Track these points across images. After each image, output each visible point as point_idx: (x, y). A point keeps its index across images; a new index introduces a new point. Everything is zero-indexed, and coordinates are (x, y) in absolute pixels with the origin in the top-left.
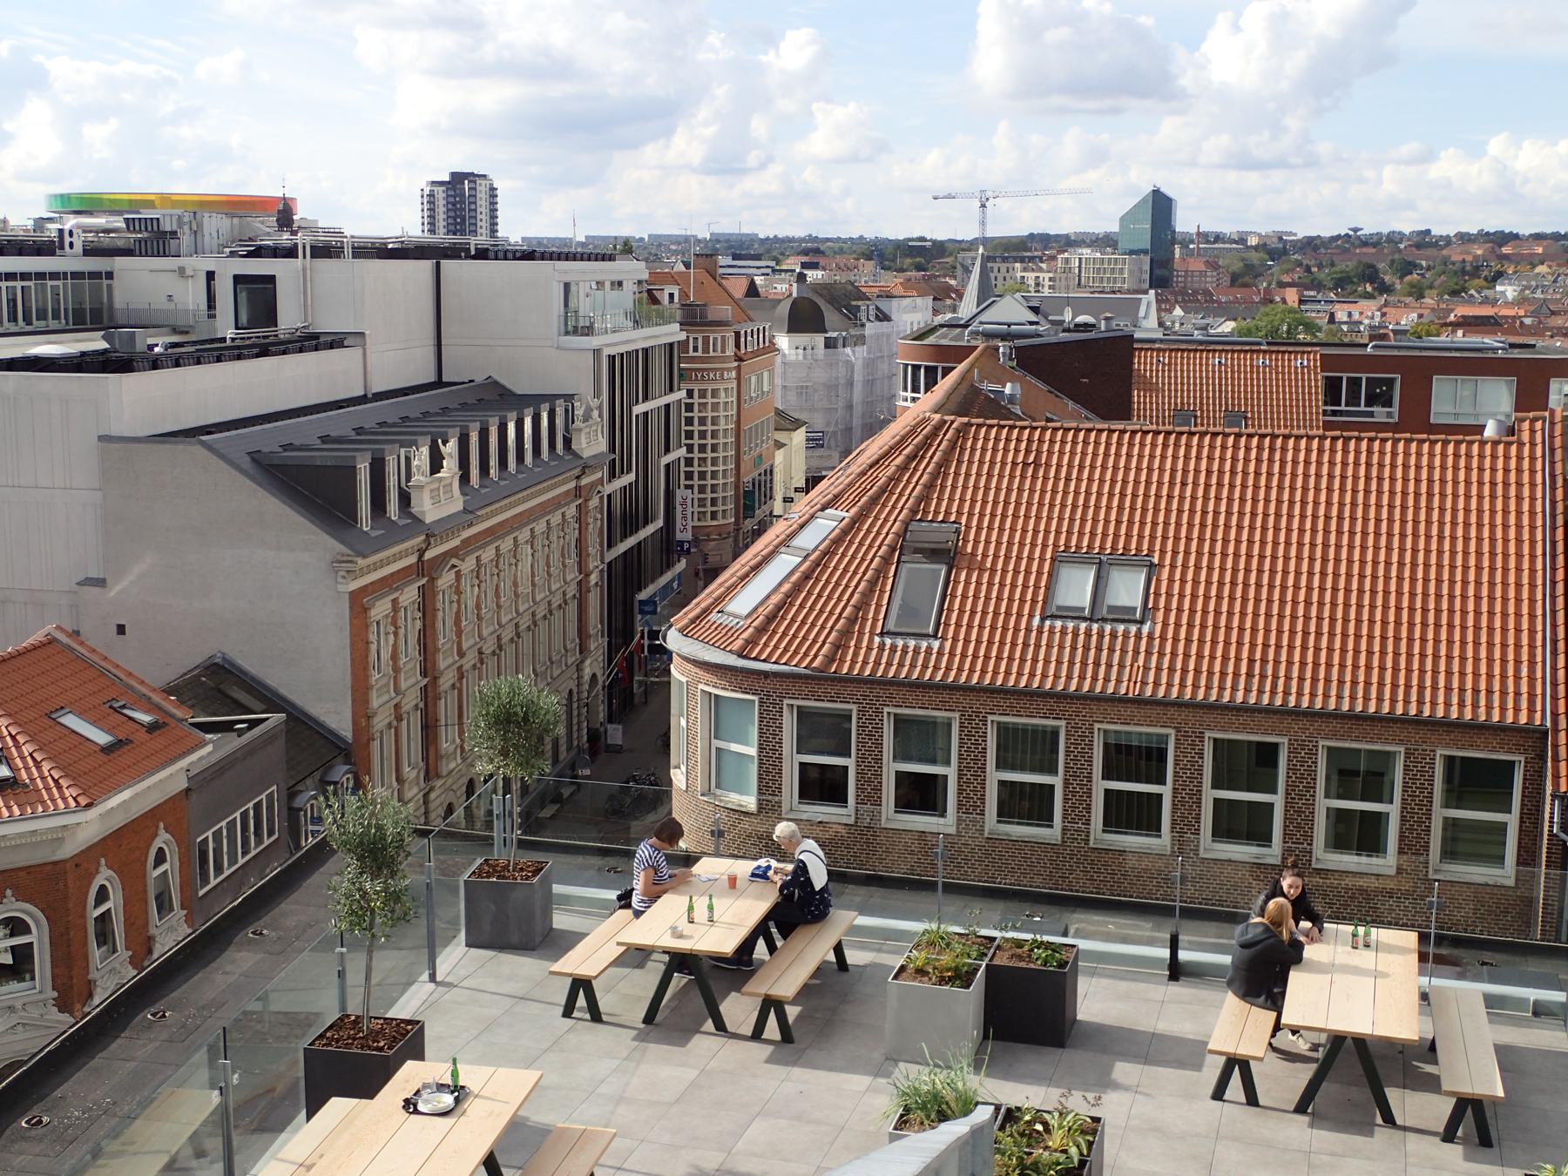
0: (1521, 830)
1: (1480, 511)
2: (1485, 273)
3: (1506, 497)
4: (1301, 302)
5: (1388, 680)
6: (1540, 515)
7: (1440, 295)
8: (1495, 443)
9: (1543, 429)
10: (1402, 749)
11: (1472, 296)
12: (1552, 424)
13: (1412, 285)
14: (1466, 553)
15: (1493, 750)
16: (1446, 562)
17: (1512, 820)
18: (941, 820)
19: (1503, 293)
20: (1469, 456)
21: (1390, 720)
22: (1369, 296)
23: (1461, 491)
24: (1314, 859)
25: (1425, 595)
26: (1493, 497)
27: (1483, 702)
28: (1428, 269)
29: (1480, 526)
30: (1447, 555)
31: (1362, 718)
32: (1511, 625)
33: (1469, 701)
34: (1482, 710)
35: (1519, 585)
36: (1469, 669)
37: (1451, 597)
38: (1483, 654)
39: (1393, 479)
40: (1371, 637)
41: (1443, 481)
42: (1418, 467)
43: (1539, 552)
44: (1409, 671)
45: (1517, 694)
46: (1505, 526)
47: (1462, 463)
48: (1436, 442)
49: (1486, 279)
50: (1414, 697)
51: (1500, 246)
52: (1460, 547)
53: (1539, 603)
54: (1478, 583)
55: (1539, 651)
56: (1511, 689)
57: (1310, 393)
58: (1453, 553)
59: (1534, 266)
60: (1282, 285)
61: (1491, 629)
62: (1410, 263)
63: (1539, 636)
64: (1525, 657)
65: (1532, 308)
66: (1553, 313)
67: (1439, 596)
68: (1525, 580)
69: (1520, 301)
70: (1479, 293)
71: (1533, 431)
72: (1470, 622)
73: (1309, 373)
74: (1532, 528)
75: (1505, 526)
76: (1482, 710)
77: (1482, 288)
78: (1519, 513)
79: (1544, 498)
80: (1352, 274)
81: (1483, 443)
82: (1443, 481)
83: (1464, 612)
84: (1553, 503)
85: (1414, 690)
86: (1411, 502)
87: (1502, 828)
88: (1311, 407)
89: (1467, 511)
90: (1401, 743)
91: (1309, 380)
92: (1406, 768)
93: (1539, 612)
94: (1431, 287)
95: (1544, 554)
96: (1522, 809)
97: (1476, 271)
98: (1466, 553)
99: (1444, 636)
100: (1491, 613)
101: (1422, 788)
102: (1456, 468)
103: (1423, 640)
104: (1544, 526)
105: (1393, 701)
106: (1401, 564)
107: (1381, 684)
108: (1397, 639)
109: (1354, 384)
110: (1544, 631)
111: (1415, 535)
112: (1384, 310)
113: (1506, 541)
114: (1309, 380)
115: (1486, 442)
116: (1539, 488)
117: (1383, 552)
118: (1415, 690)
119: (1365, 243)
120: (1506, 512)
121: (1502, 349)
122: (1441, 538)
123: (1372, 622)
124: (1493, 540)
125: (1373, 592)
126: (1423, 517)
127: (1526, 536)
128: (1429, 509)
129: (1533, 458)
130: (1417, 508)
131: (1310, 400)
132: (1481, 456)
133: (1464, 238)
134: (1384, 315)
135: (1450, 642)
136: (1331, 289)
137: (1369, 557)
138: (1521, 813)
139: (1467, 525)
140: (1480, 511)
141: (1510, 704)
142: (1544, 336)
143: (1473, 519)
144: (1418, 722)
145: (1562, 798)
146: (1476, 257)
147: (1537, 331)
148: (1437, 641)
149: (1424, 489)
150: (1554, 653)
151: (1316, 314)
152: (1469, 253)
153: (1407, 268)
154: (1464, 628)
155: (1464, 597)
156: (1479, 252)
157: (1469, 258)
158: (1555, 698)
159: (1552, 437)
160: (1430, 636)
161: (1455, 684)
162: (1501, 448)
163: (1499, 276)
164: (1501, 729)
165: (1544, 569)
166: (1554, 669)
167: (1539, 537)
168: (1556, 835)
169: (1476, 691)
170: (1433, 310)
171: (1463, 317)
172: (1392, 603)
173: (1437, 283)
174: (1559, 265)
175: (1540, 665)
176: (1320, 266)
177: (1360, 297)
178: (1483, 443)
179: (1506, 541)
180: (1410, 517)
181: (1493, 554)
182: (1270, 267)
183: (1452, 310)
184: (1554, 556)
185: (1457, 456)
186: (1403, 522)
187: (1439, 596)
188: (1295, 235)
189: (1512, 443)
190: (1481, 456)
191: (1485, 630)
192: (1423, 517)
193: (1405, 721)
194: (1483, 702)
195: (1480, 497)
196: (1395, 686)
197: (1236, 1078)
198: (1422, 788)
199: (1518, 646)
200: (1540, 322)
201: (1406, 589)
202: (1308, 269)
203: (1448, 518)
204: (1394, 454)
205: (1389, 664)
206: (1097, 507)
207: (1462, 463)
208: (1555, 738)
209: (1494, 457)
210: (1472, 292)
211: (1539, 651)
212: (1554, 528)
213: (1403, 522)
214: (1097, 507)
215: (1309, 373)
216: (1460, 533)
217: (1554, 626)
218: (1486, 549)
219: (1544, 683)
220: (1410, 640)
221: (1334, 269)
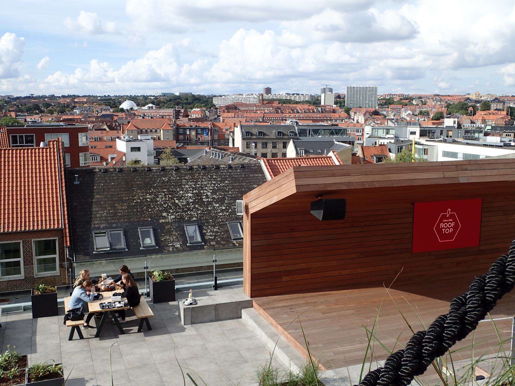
0: (60, 259)
1: (40, 168)
2: (71, 107)
3: (47, 164)
4: (16, 116)
5: (15, 221)
6: (57, 168)
7: (58, 113)
8: (43, 149)
9: (56, 144)
10: (21, 241)
11: (67, 113)
12: (59, 142)
13: (49, 110)
14: (36, 181)
15: (49, 237)
16: (30, 184)
17: (57, 256)
18: (55, 272)
19: (76, 112)
20: (35, 153)
21: (16, 233)
22: (38, 114)
23: (37, 163)
24: (35, 275)
25: (25, 194)
26: (43, 164)
27: (44, 224)
28: (54, 106)
29: (40, 173)
30: (30, 182)
31: (8, 234)
32: (51, 200)
33: (40, 224)
34: (44, 226)
35: (52, 189)
36: (39, 214)
37: (33, 194)
38: (43, 210)
39: (12, 161)
40: (8, 209)
41: (28, 161)
42: (20, 157)
43: (58, 179)
44: (21, 217)
45: (54, 220)
46: (47, 172)
47: (33, 155)
48: (25, 149)
49: (71, 108)
50: (23, 225)
51: (74, 99)
52: (34, 179)
53: (59, 193)
54: (40, 189)
55: (59, 207)
56: (52, 219)
57: (4, 140)
58: (32, 181)
59: (83, 104)
60: (10, 111)
61: (45, 202)
62: (49, 104)
63: (59, 203)
64: (55, 209)
65: (84, 116)
66: (89, 117)
67: (29, 194)
68: (54, 187)
69: (81, 114)
70: (69, 112)
71: (53, 145)
72: (39, 201)
73: (3, 134)
74: (55, 172)
75: (47, 172)
76: (44, 226)
77: (70, 111)
78: (51, 168)
79: (58, 163)
80: (32, 107)
81: (39, 149)
82: (28, 161)
83: (37, 198)
84: (60, 164)
85: (15, 224)
86: (18, 168)
87: (54, 259)
88: (5, 144)
89: (36, 169)
90: (21, 239)
91: (4, 136)
92: (23, 246)
93: (59, 196)
94: (56, 111)
95: (59, 179)
96: (59, 253)
97: (68, 106)
98: (36, 181)
99: (31, 206)
100: (45, 198)
101: (29, 252)
102: (32, 157)
103: (25, 208)
104: (58, 171)
105: (34, 226)
106: (17, 186)
107: (13, 223)
108: (17, 208)
109: (21, 137)
110: (60, 201)
111: (21, 177)
112: (41, 118)
113: (48, 176)
114: (4, 136)
115: (40, 149)
116: (56, 160)
117: (11, 183)
118: (23, 223)
119: (36, 98)
120: (47, 168)
121: (65, 125)
122: (28, 177)
123: (9, 204)
124: (44, 176)
125: (9, 195)
126: (22, 172)
127: (53, 175)
128: (24, 169)
129: (54, 152)
130: (20, 169)
131: (5, 142)
132: (39, 153)
133: (63, 97)
134: (41, 119)
135: (33, 207)
136: (26, 112)
137: (7, 185)
138: (59, 254)
139: (36, 173)
140: (40, 168)
141: (52, 223)
142: (86, 123)
143: (38, 171)
144: (25, 232)
145: (68, 247)
146: (68, 102)
147: (84, 122)
148: (29, 208)
149: (22, 163)
150: (64, 207)
151: (21, 120)
152: (66, 101)
153: (48, 105)
154: (37, 203)
155: (36, 194)
156: (69, 101)
157: (66, 103)
158: (64, 220)
159: (59, 146)
160: (27, 206)
161: (36, 220)
162: (45, 150)
163: (74, 107)
164: (50, 231)
165: (59, 183)
166: (64, 211)
167: (57, 174)
168: (68, 258)
169: (42, 221)
170: (56, 117)
171: (64, 119)
172: (15, 198)
173: (57, 110)
174: (91, 104)
175: (60, 211)
176: (22, 105)
177: (34, 114)
178: (39, 149)
179: (48, 176)
180: (18, 172)
181: (44, 181)
182: (6, 106)
183: (61, 117)
184: (62, 179)
185: (31, 153)
186: (17, 174)
187: (29, 194)
188: (13, 96)
189: (48, 148)
190: (39, 153)
191: (43, 203)
192: (22, 172)
193: (21, 232)
194: (44, 224)
195: (39, 164)
196: (17, 222)
197: (76, 332)
198: (29, 252)
199: (53, 206)
200: (86, 120)
201: (19, 193)
202: (18, 106)
203: (30, 171)
204: (12, 154)
205: (15, 216)
206: (25, 186)
207: (33, 155)
208: (65, 231)
209: (43, 153)
210: (67, 112)
211: (59, 207)
212: (61, 172)
213: (17, 174)
214: (25, 186)
215: (3, 134)
216: (34, 175)
217: (63, 199)
218: (42, 179)
219: (61, 216)
220: (21, 208)
221: (26, 106)
